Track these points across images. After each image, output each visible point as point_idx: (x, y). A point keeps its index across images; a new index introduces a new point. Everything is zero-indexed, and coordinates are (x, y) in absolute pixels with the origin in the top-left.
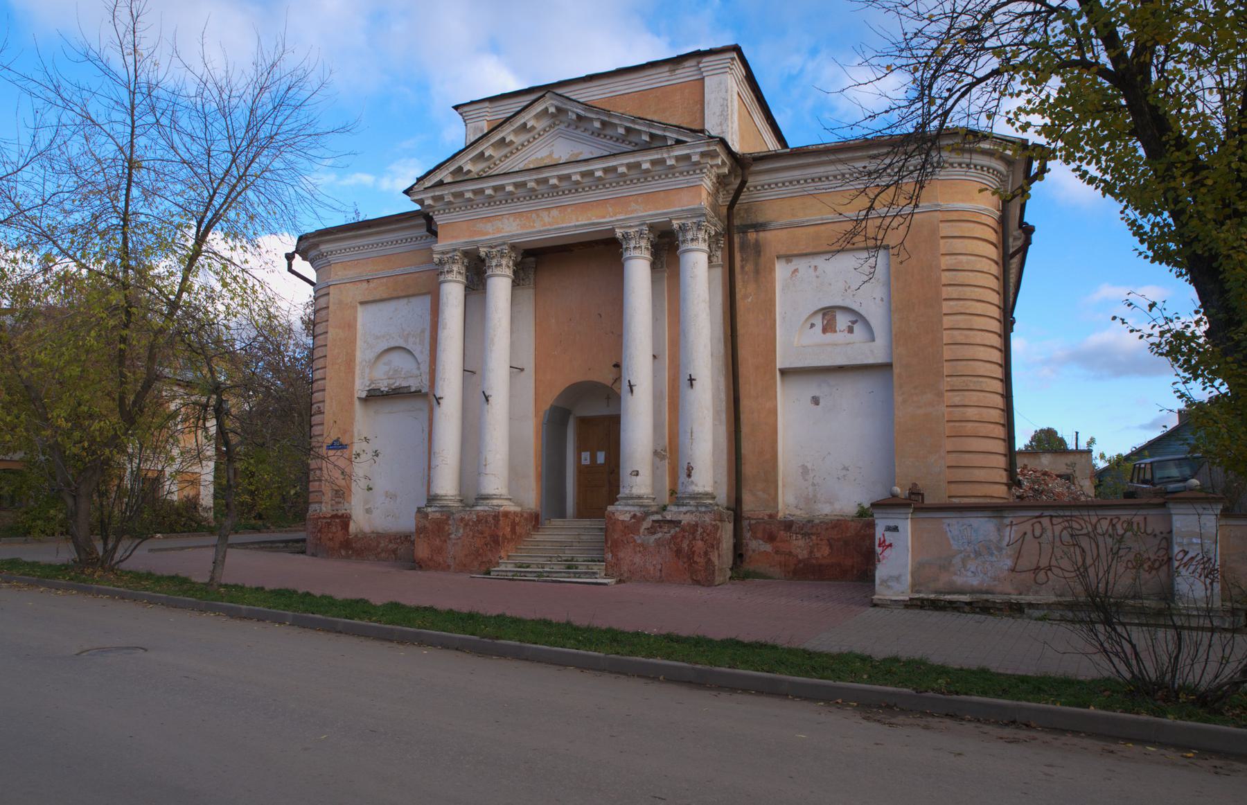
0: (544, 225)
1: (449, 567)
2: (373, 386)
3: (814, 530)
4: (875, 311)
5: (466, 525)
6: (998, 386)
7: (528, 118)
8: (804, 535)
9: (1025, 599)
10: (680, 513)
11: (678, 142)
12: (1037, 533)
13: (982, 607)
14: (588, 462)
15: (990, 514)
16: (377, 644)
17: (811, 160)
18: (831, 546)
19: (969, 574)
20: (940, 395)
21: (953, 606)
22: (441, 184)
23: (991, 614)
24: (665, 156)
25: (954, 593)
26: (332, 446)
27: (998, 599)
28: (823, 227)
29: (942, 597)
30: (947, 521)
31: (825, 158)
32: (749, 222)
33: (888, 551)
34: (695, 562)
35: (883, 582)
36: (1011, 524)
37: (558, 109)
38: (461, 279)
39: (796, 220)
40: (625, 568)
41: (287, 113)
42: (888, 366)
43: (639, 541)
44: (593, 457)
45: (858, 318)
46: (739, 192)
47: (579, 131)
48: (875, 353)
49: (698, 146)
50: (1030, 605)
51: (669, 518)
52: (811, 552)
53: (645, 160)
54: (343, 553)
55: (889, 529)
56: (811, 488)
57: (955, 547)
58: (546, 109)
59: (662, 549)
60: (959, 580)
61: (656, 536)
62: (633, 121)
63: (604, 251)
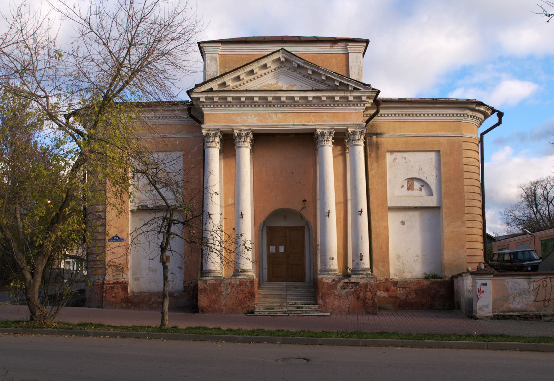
0: (274, 122)
1: (222, 310)
2: (141, 204)
3: (408, 286)
4: (432, 181)
5: (233, 287)
6: (480, 219)
7: (268, 61)
8: (403, 288)
9: (542, 313)
10: (358, 278)
11: (355, 89)
12: (545, 285)
13: (524, 317)
14: (274, 251)
15: (525, 277)
16: (289, 345)
17: (407, 106)
18: (416, 293)
19: (516, 303)
20: (464, 222)
21: (511, 317)
22: (211, 90)
23: (528, 320)
24: (349, 95)
25: (510, 312)
26: (113, 239)
27: (531, 313)
29: (506, 314)
30: (507, 280)
31: (422, 106)
33: (482, 295)
34: (367, 303)
35: (480, 308)
36: (534, 281)
38: (218, 146)
40: (330, 307)
44: (277, 249)
45: (424, 184)
46: (372, 117)
47: (295, 73)
48: (432, 202)
50: (545, 316)
51: (353, 281)
52: (407, 296)
53: (337, 95)
54: (124, 305)
55: (482, 284)
56: (401, 266)
57: (510, 292)
58: (279, 59)
59: (349, 297)
60: (512, 306)
61: (346, 290)
62: (331, 74)
63: (308, 140)
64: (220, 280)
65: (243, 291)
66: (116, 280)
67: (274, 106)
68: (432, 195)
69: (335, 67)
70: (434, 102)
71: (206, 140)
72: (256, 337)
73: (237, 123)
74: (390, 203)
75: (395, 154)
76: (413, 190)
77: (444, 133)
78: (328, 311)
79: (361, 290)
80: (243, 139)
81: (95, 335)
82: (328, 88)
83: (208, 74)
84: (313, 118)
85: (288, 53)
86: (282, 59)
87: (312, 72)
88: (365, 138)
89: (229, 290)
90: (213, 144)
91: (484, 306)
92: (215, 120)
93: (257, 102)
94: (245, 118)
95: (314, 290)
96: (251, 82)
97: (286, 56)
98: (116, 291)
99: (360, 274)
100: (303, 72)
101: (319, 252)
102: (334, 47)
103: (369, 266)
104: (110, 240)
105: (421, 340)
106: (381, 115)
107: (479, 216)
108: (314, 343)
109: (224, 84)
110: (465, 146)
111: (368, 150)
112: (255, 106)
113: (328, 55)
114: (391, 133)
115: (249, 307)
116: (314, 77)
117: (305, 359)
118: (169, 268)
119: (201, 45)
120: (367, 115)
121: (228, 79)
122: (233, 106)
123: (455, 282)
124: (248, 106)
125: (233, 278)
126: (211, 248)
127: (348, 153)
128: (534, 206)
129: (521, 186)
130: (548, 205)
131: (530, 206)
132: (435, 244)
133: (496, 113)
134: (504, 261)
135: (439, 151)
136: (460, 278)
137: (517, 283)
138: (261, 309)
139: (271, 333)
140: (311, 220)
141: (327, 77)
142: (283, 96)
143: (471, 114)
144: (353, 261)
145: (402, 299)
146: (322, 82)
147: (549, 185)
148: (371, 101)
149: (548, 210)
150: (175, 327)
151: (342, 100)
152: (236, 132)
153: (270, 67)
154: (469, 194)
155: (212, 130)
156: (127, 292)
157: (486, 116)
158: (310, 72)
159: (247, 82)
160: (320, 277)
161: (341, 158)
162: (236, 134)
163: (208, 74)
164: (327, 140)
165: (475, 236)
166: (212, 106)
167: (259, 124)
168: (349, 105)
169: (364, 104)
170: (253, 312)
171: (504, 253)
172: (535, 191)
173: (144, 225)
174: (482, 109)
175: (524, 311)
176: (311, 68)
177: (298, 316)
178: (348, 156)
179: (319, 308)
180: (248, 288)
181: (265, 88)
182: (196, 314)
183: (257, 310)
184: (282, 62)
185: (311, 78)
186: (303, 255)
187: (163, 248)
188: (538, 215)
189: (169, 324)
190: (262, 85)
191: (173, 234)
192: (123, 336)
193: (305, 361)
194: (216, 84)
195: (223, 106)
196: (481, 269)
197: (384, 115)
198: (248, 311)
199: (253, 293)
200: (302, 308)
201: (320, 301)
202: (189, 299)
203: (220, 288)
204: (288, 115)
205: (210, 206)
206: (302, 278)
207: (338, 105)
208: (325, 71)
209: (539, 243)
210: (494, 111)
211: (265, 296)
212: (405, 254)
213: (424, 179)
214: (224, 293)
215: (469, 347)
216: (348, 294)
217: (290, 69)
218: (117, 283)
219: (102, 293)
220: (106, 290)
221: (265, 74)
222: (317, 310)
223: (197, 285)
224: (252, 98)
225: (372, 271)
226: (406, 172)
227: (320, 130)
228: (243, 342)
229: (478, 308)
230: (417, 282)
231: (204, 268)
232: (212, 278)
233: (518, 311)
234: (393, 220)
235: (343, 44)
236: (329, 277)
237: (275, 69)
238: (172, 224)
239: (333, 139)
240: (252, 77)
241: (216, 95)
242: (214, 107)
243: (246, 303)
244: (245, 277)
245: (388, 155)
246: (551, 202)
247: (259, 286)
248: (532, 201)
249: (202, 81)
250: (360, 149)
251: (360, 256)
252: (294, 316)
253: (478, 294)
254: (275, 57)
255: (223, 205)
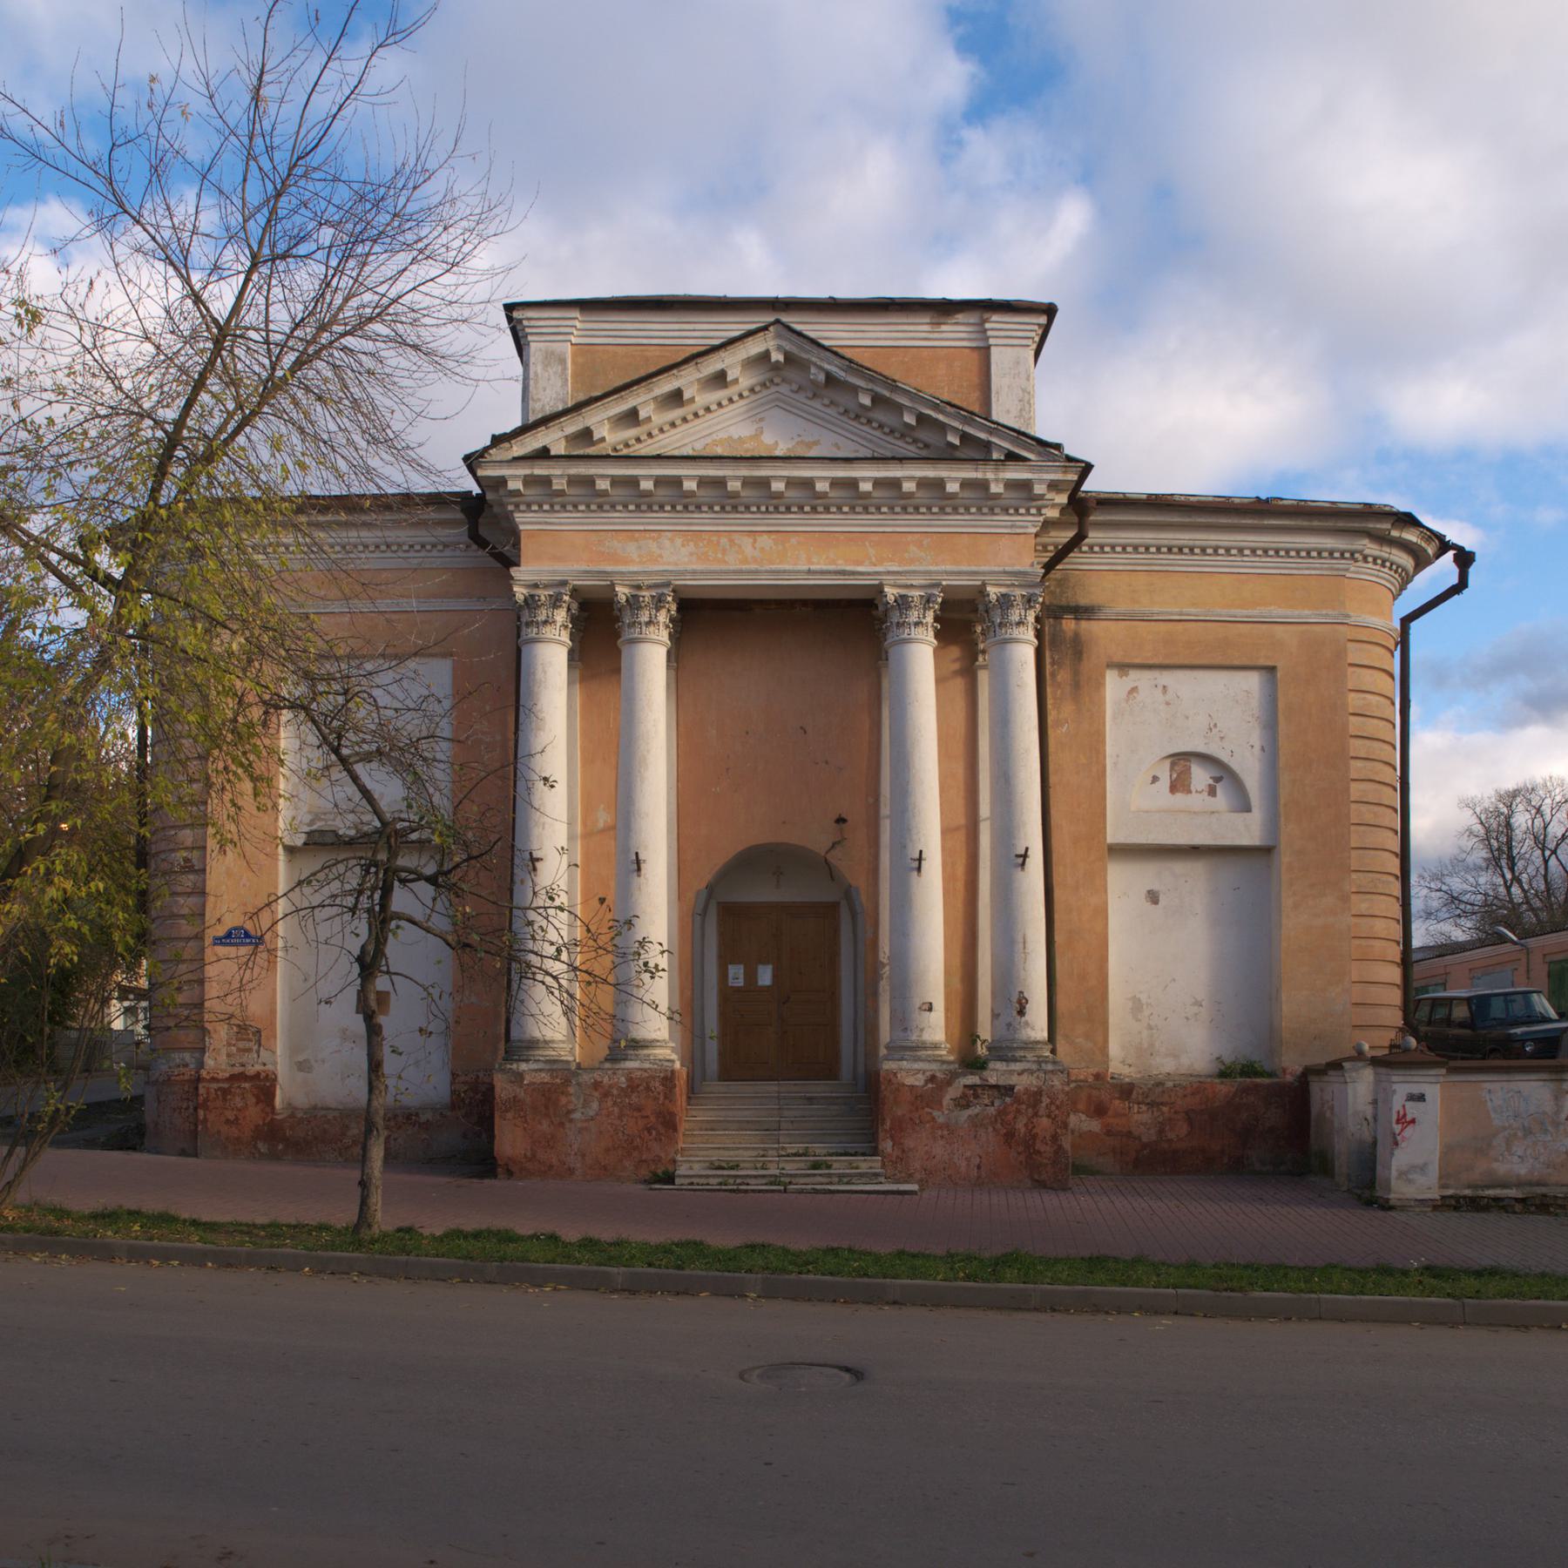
0: (745, 561)
1: (571, 1171)
3: (1166, 1098)
4: (1249, 766)
5: (606, 1095)
6: (1396, 888)
7: (729, 363)
8: (1151, 1105)
10: (1011, 1072)
11: (1011, 457)
14: (740, 983)
15: (1545, 1076)
17: (1176, 519)
19: (1515, 1159)
20: (1345, 899)
21: (1499, 1204)
22: (543, 454)
23: (1549, 1213)
24: (990, 476)
28: (1180, 626)
29: (1480, 1193)
31: (1223, 520)
32: (1064, 602)
33: (1409, 1131)
35: (1402, 1174)
37: (789, 357)
38: (565, 637)
39: (1137, 608)
40: (917, 1165)
41: (433, 273)
42: (1265, 852)
43: (941, 1120)
44: (751, 976)
45: (1223, 773)
47: (817, 404)
48: (1247, 830)
49: (1047, 469)
51: (992, 1081)
52: (1161, 1132)
53: (954, 477)
55: (1412, 1098)
56: (1145, 1033)
58: (765, 356)
62: (936, 407)
63: (851, 623)
64: (564, 1074)
65: (639, 1109)
66: (238, 1070)
67: (747, 508)
68: (1248, 809)
69: (948, 385)
70: (1260, 512)
71: (525, 617)
72: (679, 1269)
73: (626, 562)
74: (1115, 833)
75: (1135, 677)
76: (1189, 792)
77: (1289, 612)
78: (911, 1175)
79: (1018, 1111)
80: (542, 615)
81: (138, 1255)
82: (924, 453)
83: (538, 406)
84: (872, 552)
85: (794, 337)
86: (777, 357)
87: (873, 400)
88: (1037, 619)
89: (595, 1105)
90: (548, 632)
91: (1413, 1168)
92: (558, 551)
93: (691, 494)
94: (653, 546)
95: (869, 1111)
96: (674, 431)
97: (788, 346)
98: (238, 1102)
99: (1015, 1060)
100: (844, 399)
101: (884, 986)
102: (944, 328)
103: (1045, 1034)
104: (219, 941)
105: (1241, 1290)
106: (1091, 547)
107: (1392, 879)
108: (874, 1298)
109: (586, 435)
110: (1355, 654)
111: (1048, 660)
112: (686, 507)
113: (925, 353)
114: (1122, 607)
115: (658, 1160)
116: (880, 416)
117: (847, 1370)
118: (386, 1032)
119: (516, 314)
120: (1045, 546)
121: (599, 420)
122: (613, 506)
123: (1315, 1088)
124: (662, 507)
125: (607, 1065)
126: (529, 966)
127: (984, 667)
128: (1504, 863)
129: (1469, 804)
130: (1546, 861)
131: (1494, 862)
132: (1253, 966)
133: (1451, 554)
134: (1448, 1022)
135: (1272, 670)
136: (1333, 1076)
137: (1519, 1095)
138: (697, 1169)
139: (727, 1259)
140: (859, 881)
141: (921, 418)
142: (779, 477)
143: (1377, 553)
144: (995, 1016)
145: (1145, 1140)
146: (905, 432)
147: (1548, 801)
148: (1063, 499)
149: (1545, 877)
150: (409, 1230)
151: (967, 494)
152: (622, 592)
153: (736, 381)
154: (1364, 808)
155: (546, 587)
156: (273, 1107)
157: (1422, 561)
158: (866, 400)
159: (661, 430)
160: (888, 1066)
161: (959, 684)
162: (623, 599)
163: (538, 406)
164: (917, 624)
165: (1378, 944)
166: (546, 507)
167: (699, 567)
168: (992, 511)
169: (1039, 509)
170: (669, 1179)
171: (1452, 999)
172: (1508, 818)
173: (300, 883)
174: (1411, 536)
175: (1538, 1184)
176: (870, 386)
177: (816, 1191)
178: (983, 677)
179: (883, 1166)
180: (656, 1099)
181: (719, 451)
182: (487, 1181)
183: (682, 1170)
184: (776, 367)
185: (869, 422)
186: (833, 996)
187: (369, 964)
188: (1515, 890)
189: (384, 1219)
190: (709, 440)
191: (399, 916)
192: (227, 1262)
193: (847, 1376)
194: (560, 434)
195: (582, 507)
196: (1407, 1050)
197: (1102, 547)
198: (655, 1174)
199: (672, 1114)
200: (829, 1167)
201: (887, 1145)
202: (466, 1132)
203: (564, 1100)
204: (793, 540)
205: (536, 831)
206: (829, 1071)
207: (955, 510)
208: (915, 396)
209: (1540, 971)
210: (1444, 546)
211: (712, 1126)
212: (1158, 992)
213: (1224, 756)
214: (577, 1116)
215: (1400, 1317)
216: (975, 1123)
217: (800, 388)
218: (241, 1077)
219: (196, 1109)
220: (206, 1100)
221: (720, 405)
222: (876, 1175)
223: (491, 1088)
224: (677, 482)
225: (1053, 1051)
226: (1168, 731)
227: (896, 591)
228: (631, 1289)
229: (1394, 1173)
230: (1195, 1086)
231: (514, 1034)
232: (541, 1066)
233: (1520, 1184)
234: (1123, 887)
235: (972, 318)
236: (916, 1066)
237: (752, 390)
238: (396, 883)
239: (936, 619)
240: (676, 414)
241: (558, 472)
242: (552, 510)
243: (648, 1149)
244: (647, 1065)
245: (1111, 677)
246: (1554, 852)
247: (692, 1092)
248: (1499, 849)
249: (516, 422)
250: (1024, 654)
251: (1019, 1002)
252: (801, 1192)
253: (1397, 1128)
254: (754, 347)
255: (579, 829)
